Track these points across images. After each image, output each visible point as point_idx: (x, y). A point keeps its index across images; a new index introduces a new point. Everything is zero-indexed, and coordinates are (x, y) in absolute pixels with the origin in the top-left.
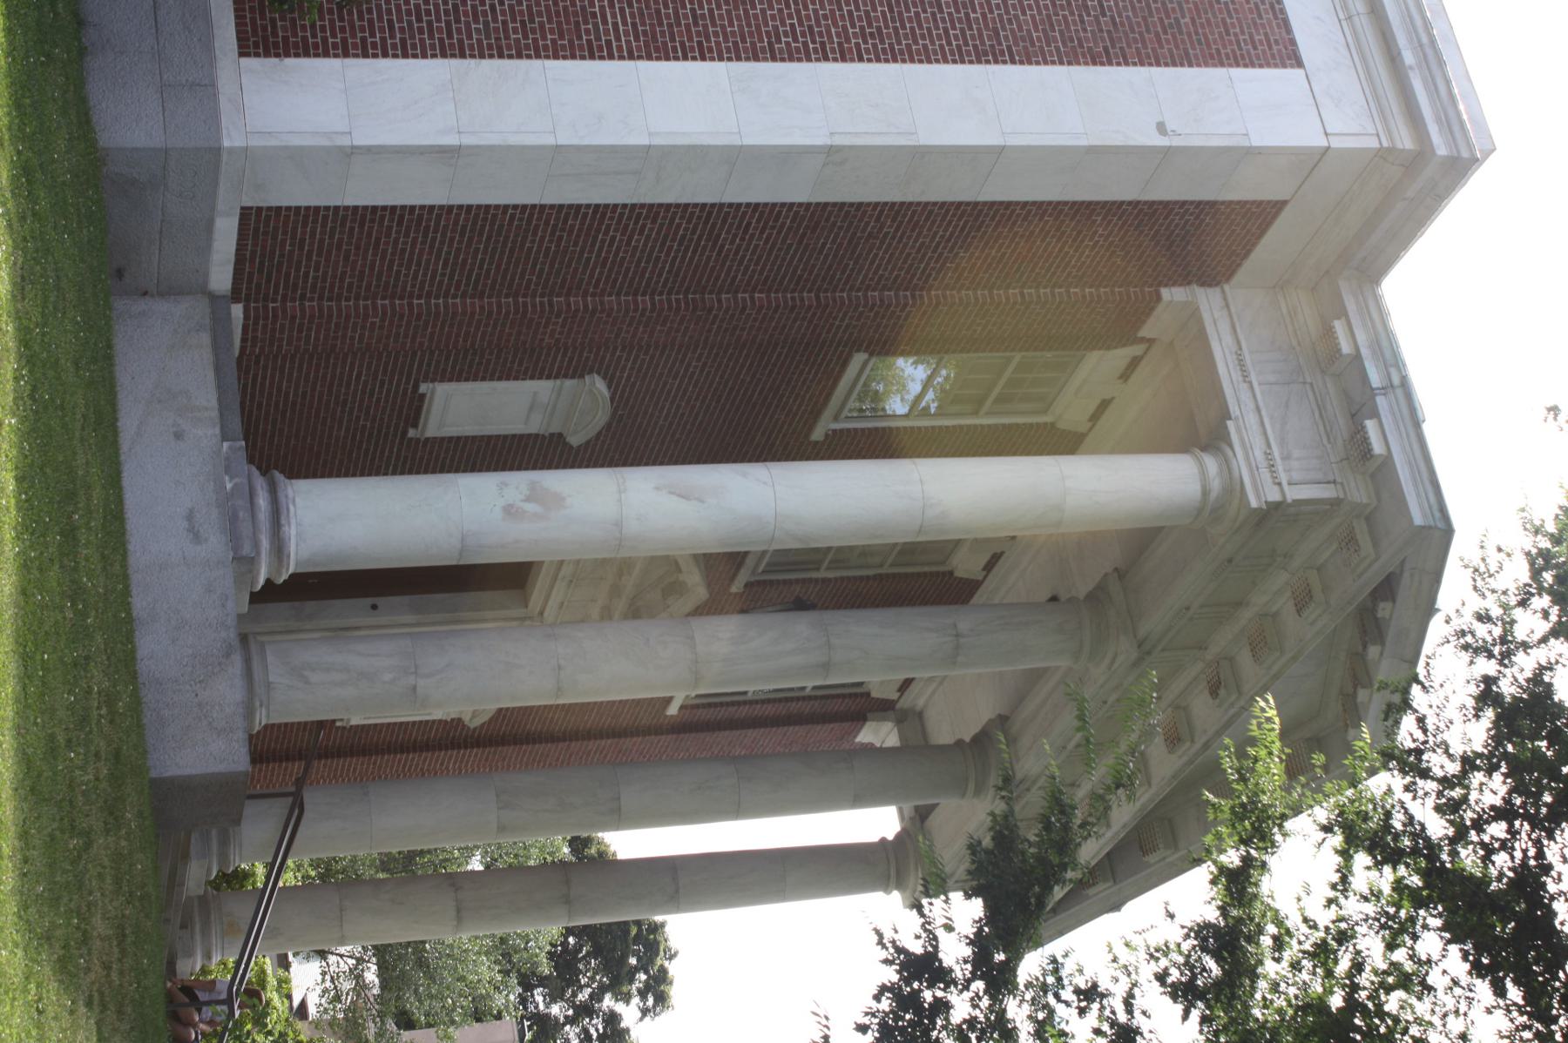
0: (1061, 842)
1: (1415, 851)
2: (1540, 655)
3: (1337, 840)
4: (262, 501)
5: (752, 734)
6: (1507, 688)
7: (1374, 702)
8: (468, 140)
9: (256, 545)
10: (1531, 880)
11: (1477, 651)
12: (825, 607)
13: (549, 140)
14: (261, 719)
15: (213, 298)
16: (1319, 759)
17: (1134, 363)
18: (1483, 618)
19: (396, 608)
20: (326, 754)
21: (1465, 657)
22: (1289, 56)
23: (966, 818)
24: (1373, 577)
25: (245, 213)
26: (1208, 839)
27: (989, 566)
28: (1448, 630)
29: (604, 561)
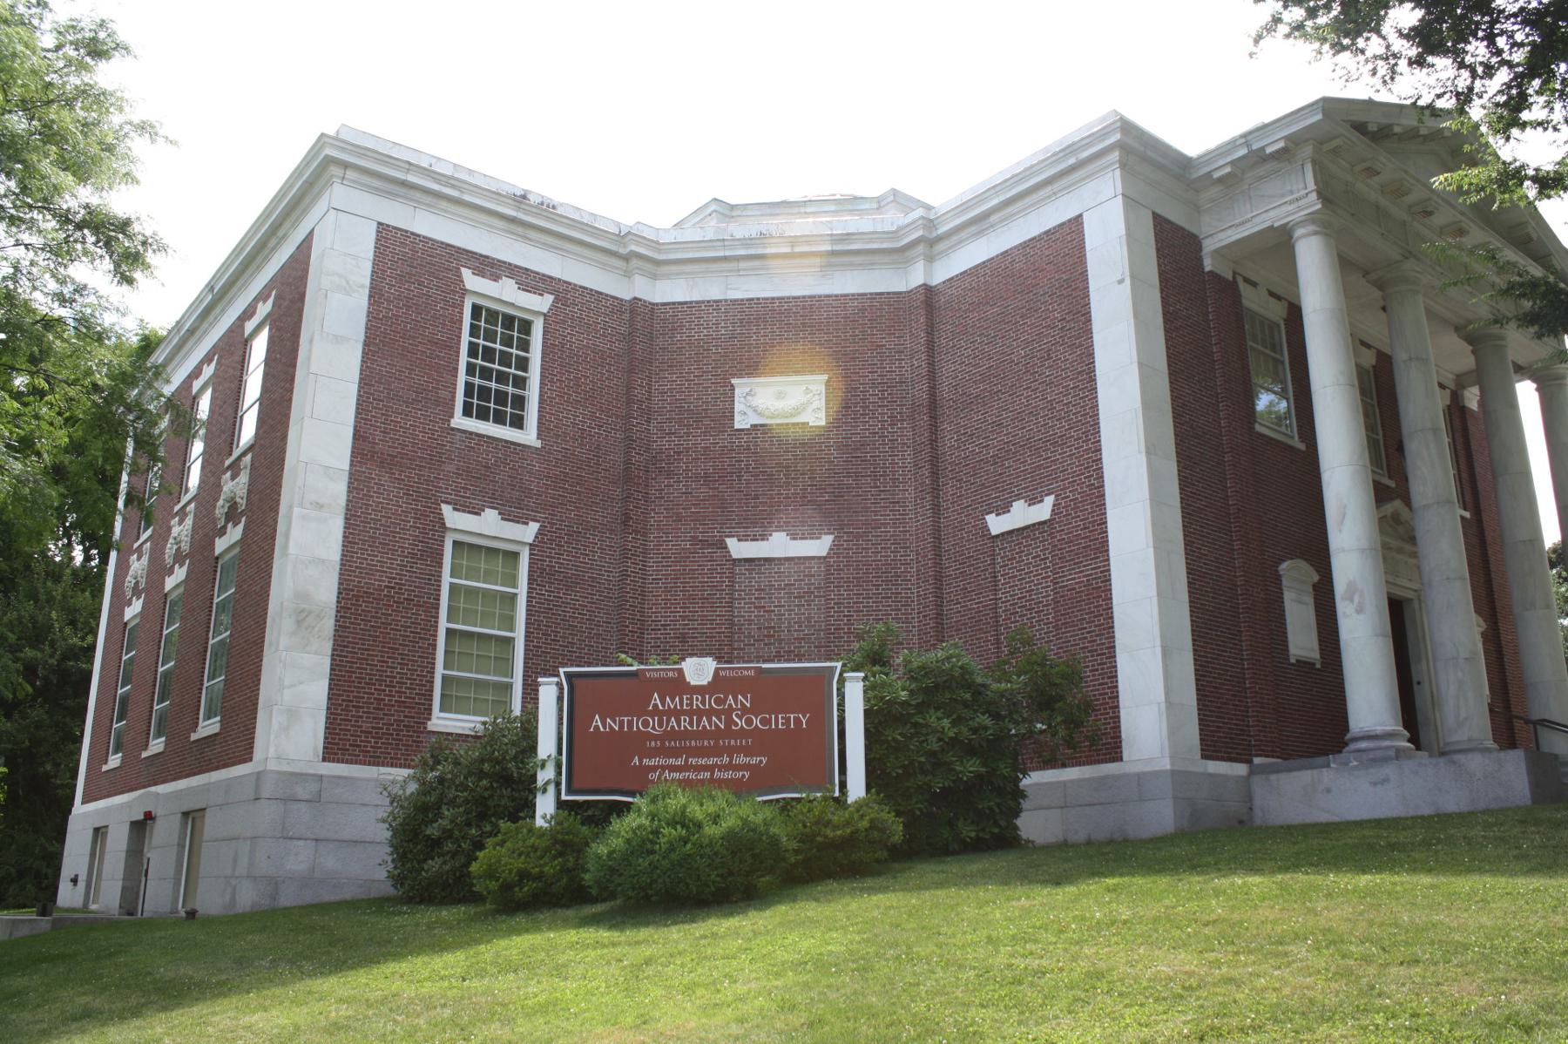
0: (1531, 287)
1: (1519, 86)
2: (1393, 38)
3: (1515, 132)
4: (1363, 745)
5: (1478, 469)
6: (1414, 52)
7: (1430, 123)
8: (1158, 642)
9: (1388, 748)
10: (1528, 18)
11: (1394, 72)
12: (1400, 435)
13: (1155, 600)
14: (1490, 744)
15: (1251, 773)
16: (1467, 148)
17: (1247, 280)
18: (1374, 72)
19: (1418, 670)
20: (1507, 706)
21: (1398, 78)
22: (1078, 219)
23: (1519, 343)
24: (1355, 136)
25: (1204, 757)
26: (1522, 204)
27: (1368, 346)
28: (1383, 90)
29: (1385, 559)
